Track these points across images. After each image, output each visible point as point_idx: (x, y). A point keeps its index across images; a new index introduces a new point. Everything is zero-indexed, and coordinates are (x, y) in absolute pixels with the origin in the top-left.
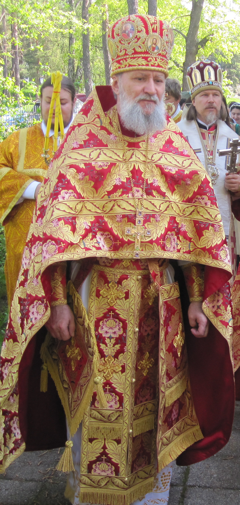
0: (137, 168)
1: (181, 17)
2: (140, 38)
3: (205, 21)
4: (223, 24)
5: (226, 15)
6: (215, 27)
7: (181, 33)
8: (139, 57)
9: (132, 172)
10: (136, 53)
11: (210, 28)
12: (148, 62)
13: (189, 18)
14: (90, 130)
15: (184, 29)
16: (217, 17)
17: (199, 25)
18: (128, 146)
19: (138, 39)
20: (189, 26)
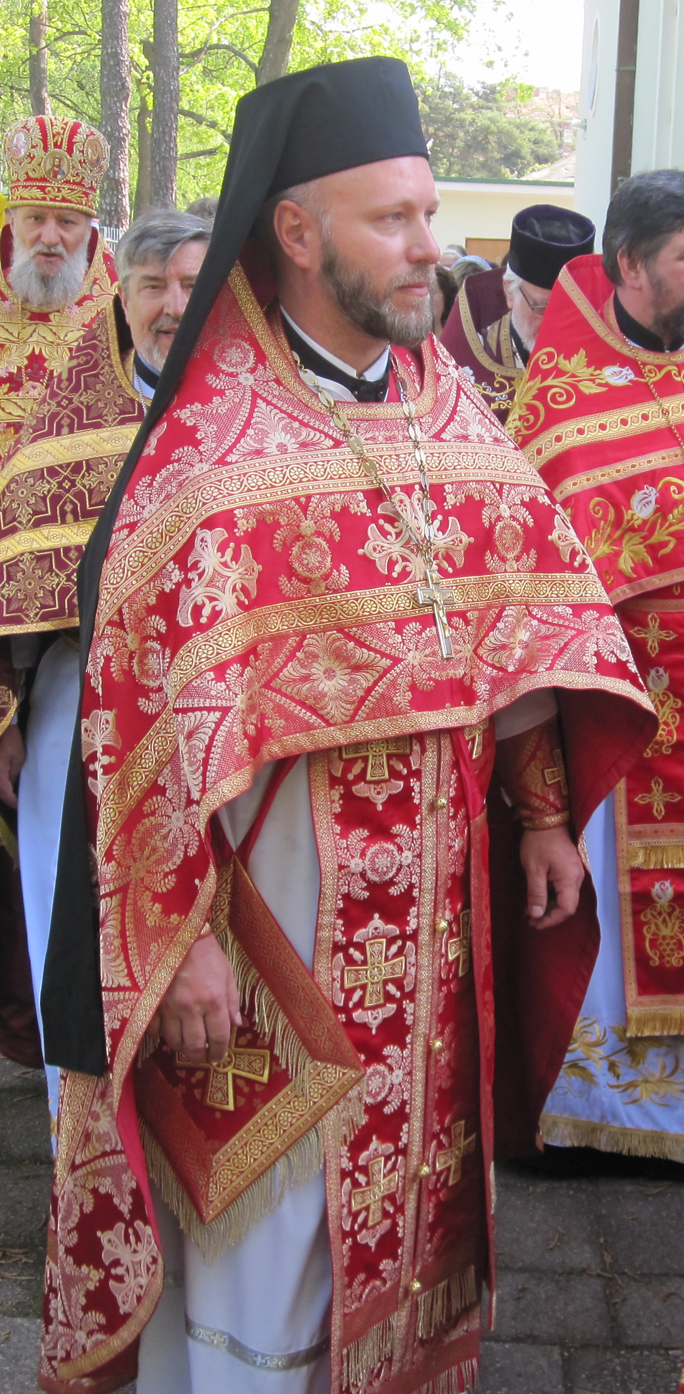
0: (37, 352)
1: (245, 13)
2: (34, 157)
3: (308, 25)
4: (357, 34)
5: (366, 10)
6: (334, 42)
7: (245, 58)
8: (33, 186)
9: (28, 358)
10: (29, 179)
11: (322, 44)
12: (45, 193)
13: (266, 16)
14: (111, 285)
15: (251, 46)
16: (340, 15)
17: (291, 37)
18: (31, 319)
19: (32, 158)
20: (264, 38)
